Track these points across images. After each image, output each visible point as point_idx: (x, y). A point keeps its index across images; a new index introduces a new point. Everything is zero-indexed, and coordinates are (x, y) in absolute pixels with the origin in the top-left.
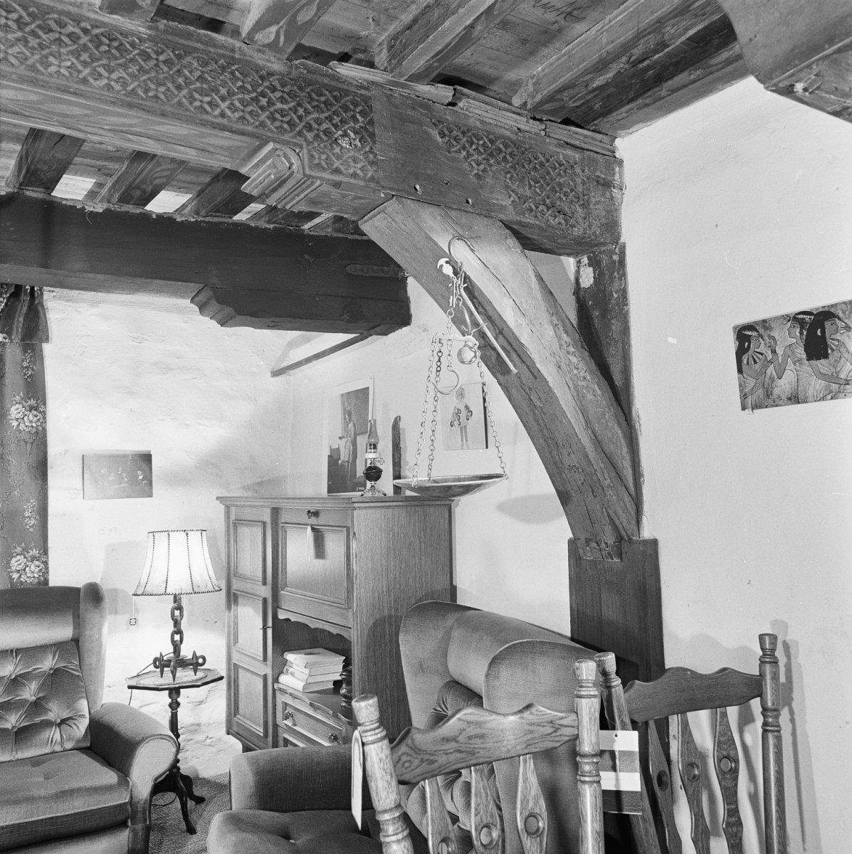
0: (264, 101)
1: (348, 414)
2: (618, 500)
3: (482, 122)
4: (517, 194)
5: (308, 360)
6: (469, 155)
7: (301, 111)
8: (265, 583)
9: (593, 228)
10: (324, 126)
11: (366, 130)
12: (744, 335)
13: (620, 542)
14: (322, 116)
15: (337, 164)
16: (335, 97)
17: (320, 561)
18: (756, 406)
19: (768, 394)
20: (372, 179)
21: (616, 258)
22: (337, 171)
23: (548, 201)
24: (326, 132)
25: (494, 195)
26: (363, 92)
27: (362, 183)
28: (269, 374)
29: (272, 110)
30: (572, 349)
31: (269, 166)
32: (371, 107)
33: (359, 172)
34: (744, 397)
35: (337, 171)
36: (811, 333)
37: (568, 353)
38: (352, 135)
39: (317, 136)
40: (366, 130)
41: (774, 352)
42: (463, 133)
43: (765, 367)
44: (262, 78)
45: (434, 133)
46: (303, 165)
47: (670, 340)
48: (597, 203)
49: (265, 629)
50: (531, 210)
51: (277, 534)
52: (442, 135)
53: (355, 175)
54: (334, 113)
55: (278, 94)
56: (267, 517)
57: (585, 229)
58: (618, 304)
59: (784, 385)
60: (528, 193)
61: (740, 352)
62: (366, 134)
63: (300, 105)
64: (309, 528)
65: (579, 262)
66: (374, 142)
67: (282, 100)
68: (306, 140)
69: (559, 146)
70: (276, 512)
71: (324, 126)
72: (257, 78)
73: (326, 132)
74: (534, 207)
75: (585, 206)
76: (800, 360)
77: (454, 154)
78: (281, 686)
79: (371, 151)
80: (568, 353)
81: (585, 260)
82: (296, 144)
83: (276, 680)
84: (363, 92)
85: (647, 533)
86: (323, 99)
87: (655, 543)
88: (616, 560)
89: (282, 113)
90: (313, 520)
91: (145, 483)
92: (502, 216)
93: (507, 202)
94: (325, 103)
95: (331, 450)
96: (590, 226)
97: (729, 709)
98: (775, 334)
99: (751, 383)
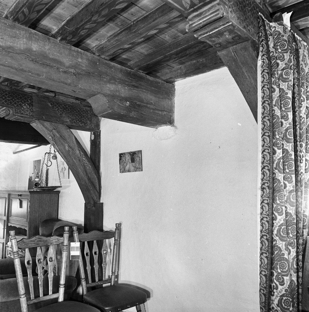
0: (4, 98)
1: (35, 167)
2: (94, 193)
3: (63, 101)
4: (71, 118)
5: (24, 150)
6: (58, 109)
7: (14, 100)
8: (5, 216)
9: (92, 126)
10: (20, 103)
11: (31, 104)
12: (121, 155)
13: (95, 203)
14: (19, 101)
15: (22, 112)
16: (23, 96)
17: (21, 209)
18: (122, 172)
19: (124, 170)
20: (32, 115)
21: (99, 133)
22: (22, 114)
23: (80, 120)
24: (20, 104)
25: (65, 119)
26: (30, 95)
27: (29, 116)
28: (12, 153)
29: (6, 99)
30: (84, 156)
31: (4, 112)
32: (32, 98)
33: (28, 114)
34: (120, 170)
35: (22, 114)
36: (132, 157)
37: (83, 157)
38: (27, 105)
39: (17, 106)
40: (31, 104)
41: (126, 160)
42: (57, 104)
43: (124, 163)
44: (4, 92)
45: (49, 104)
46: (13, 112)
47: (239, 124)
48: (94, 120)
49: (4, 229)
50: (75, 122)
51: (10, 201)
52: (51, 104)
53: (27, 115)
54: (22, 100)
55: (8, 96)
56: (7, 196)
57: (90, 127)
58: (98, 145)
59: (127, 168)
60: (74, 118)
61: (120, 159)
62: (31, 105)
63: (13, 98)
64: (18, 199)
65: (91, 133)
66: (33, 106)
67: (9, 97)
68: (14, 106)
69: (84, 106)
70: (9, 195)
71: (20, 103)
72: (2, 92)
73: (20, 104)
74: (76, 121)
75: (90, 121)
76: (130, 162)
77: (54, 109)
78: (8, 245)
79: (32, 109)
80: (83, 157)
81: (92, 133)
82: (12, 107)
83: (6, 244)
84: (30, 95)
85: (101, 202)
86: (20, 97)
87: (102, 203)
88: (94, 208)
89: (8, 100)
90: (20, 197)
91: (187, 7)
92: (66, 124)
93: (68, 120)
94: (20, 97)
95: (30, 177)
96: (91, 126)
97: (107, 240)
98: (126, 156)
99: (122, 167)
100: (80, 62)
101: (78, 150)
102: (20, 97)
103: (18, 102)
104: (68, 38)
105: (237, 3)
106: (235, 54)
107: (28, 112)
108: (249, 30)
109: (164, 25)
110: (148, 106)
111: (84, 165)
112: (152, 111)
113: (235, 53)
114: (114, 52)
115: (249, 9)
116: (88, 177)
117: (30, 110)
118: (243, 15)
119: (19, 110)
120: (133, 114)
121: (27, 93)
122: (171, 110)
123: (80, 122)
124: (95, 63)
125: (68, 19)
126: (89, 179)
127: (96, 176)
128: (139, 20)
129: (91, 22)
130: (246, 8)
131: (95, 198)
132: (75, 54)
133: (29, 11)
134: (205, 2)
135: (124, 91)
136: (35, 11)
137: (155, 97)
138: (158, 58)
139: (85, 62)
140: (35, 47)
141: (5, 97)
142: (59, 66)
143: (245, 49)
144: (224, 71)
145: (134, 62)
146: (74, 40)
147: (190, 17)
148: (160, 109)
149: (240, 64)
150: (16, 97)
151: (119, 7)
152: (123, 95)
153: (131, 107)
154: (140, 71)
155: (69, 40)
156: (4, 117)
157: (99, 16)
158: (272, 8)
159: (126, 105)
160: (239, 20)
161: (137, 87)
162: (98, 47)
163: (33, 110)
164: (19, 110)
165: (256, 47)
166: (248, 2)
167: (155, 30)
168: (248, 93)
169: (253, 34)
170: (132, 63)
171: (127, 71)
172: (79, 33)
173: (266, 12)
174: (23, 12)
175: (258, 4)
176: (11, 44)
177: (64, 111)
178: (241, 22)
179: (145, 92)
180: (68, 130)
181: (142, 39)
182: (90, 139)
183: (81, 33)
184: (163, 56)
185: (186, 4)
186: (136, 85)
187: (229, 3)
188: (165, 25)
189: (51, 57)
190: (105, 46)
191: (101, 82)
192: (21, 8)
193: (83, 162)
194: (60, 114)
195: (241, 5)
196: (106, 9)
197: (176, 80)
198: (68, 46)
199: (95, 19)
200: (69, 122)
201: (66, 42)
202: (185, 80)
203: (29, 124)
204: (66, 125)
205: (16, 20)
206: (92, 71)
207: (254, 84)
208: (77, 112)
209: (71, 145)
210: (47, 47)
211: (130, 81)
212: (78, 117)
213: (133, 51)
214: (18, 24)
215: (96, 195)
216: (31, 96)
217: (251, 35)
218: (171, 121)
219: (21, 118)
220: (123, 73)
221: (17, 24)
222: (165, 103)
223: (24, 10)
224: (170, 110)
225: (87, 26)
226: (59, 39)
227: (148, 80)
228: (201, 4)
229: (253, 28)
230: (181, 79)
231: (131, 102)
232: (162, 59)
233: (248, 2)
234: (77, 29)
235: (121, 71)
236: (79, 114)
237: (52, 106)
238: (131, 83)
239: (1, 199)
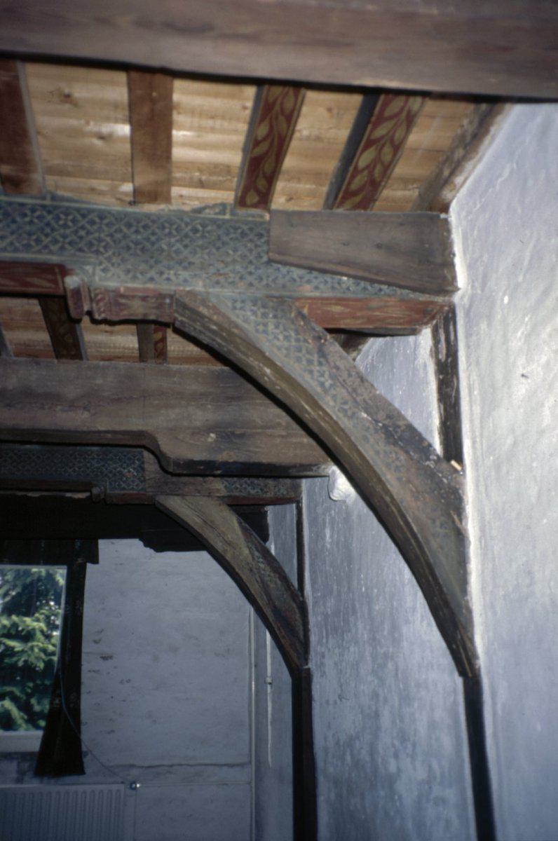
9: (281, 491)
20: (142, 489)
22: (124, 489)
30: (261, 560)
37: (259, 562)
50: (237, 488)
71: (118, 469)
74: (238, 486)
80: (259, 562)
92: (219, 495)
96: (279, 490)
110: (269, 431)
111: (263, 581)
112: (278, 440)
116: (275, 607)
152: (198, 424)
193: (259, 572)
200: (223, 489)
204: (218, 497)
209: (230, 539)
239: (500, 834)
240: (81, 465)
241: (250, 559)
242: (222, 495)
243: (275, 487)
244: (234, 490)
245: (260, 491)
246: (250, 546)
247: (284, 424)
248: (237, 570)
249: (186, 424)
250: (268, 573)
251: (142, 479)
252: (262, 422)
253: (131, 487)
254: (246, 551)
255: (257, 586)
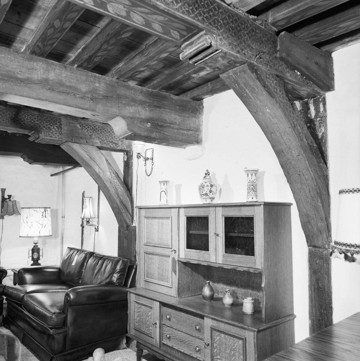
0: (33, 121)
2: (126, 216)
6: (88, 130)
7: (42, 123)
9: (124, 147)
10: (48, 126)
16: (51, 119)
20: (60, 138)
21: (131, 154)
26: (59, 117)
27: (57, 139)
29: (35, 123)
30: (115, 178)
33: (57, 136)
35: (51, 137)
38: (56, 128)
39: (46, 129)
40: (59, 126)
44: (32, 116)
45: (78, 126)
50: (105, 143)
52: (80, 126)
53: (56, 137)
55: (36, 119)
60: (105, 139)
65: (124, 154)
66: (62, 129)
67: (37, 121)
71: (48, 126)
73: (49, 128)
74: (106, 142)
81: (125, 153)
86: (48, 120)
88: (127, 231)
92: (97, 145)
94: (49, 121)
96: (123, 146)
100: (97, 87)
101: (109, 171)
102: (48, 120)
103: (47, 125)
104: (84, 65)
105: (229, 29)
106: (236, 76)
107: (57, 135)
108: (244, 54)
109: (172, 49)
110: (172, 126)
111: (115, 187)
112: (176, 131)
113: (235, 75)
114: (132, 75)
115: (245, 32)
117: (59, 132)
118: (236, 40)
119: (48, 133)
120: (254, 114)
121: (56, 115)
122: (197, 130)
123: (111, 142)
124: (113, 86)
125: (82, 47)
126: (121, 202)
127: (128, 199)
128: (150, 44)
129: (102, 51)
130: (242, 32)
131: (128, 221)
132: (92, 79)
133: (44, 45)
134: (192, 33)
135: (144, 113)
136: (48, 45)
137: (179, 116)
138: (178, 78)
139: (103, 87)
140: (52, 76)
141: (34, 121)
142: (76, 93)
143: (244, 71)
144: (231, 93)
145: (157, 81)
146: (90, 66)
147: (183, 46)
148: (185, 129)
149: (243, 86)
150: (45, 120)
151: (125, 36)
152: (143, 117)
153: (152, 128)
154: (163, 90)
155: (85, 67)
156: (34, 140)
157: (108, 45)
158: (276, 27)
159: (147, 127)
160: (231, 46)
161: (159, 107)
162: (116, 70)
163: (62, 132)
164: (48, 133)
165: (255, 69)
166: (245, 26)
167: (165, 53)
168: (256, 113)
169: (250, 57)
170: (155, 83)
171: (148, 91)
172: (93, 60)
173: (270, 32)
174: (38, 46)
175: (259, 25)
176: (28, 76)
177: (94, 133)
178: (234, 48)
179: (169, 112)
180: (98, 152)
181: (156, 62)
182: (123, 160)
183: (95, 59)
184: (182, 75)
185: (175, 36)
186: (158, 106)
187: (218, 32)
188: (174, 48)
189: (68, 84)
190: (122, 70)
191: (120, 105)
192: (36, 42)
194: (90, 136)
195: (234, 31)
196: (112, 39)
197: (203, 97)
198: (85, 72)
199: (105, 48)
200: (99, 143)
201: (83, 68)
202: (213, 96)
203: (59, 146)
204: (96, 146)
205: (33, 53)
206: (110, 94)
207: (259, 104)
208: (107, 133)
210: (64, 75)
211: (151, 101)
212: (109, 138)
213: (153, 71)
214: (35, 56)
215: (128, 218)
216: (60, 119)
217: (248, 58)
218: (198, 140)
219: (51, 141)
220: (144, 94)
221: (34, 56)
222: (191, 122)
223: (39, 44)
224: (197, 129)
225: (99, 54)
226: (76, 66)
227: (173, 99)
228: (190, 35)
229: (251, 51)
230: (209, 96)
231: (153, 123)
232: (181, 79)
233: (243, 26)
234: (90, 57)
235: (142, 92)
236: (110, 135)
237: (81, 127)
238: (153, 103)
240: (28, 121)
241: (110, 177)
242: (98, 146)
243: (122, 144)
244: (104, 144)
245: (115, 146)
246: (111, 171)
247: (178, 123)
248: (105, 182)
249: (137, 115)
250: (118, 184)
251: (60, 132)
252: (169, 121)
253: (55, 136)
254: (109, 174)
255: (113, 190)
